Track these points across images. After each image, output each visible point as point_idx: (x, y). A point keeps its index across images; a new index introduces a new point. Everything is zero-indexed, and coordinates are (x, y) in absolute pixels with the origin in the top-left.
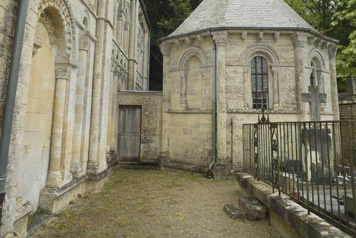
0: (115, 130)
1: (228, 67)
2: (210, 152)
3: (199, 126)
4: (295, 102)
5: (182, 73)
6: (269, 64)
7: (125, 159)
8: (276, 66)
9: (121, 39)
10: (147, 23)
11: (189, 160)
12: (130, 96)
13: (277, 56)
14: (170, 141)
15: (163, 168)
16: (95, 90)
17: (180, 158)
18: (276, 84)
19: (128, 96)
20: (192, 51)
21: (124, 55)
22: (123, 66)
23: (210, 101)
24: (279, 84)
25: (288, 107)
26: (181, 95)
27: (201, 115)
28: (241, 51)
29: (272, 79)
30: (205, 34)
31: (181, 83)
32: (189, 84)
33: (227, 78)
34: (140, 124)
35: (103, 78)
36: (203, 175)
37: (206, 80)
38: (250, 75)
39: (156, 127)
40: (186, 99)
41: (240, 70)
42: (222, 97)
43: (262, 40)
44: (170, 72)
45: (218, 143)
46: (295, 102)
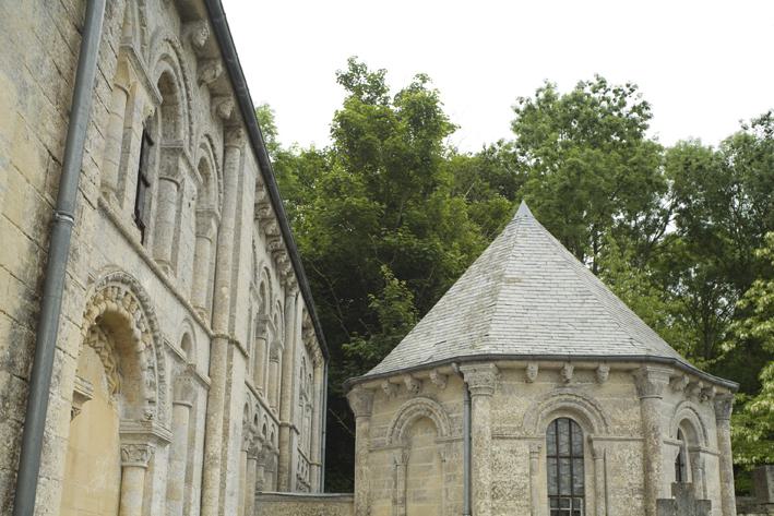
1: (496, 441)
5: (397, 454)
6: (586, 435)
8: (602, 439)
9: (264, 382)
12: (284, 504)
13: (603, 418)
16: (208, 492)
18: (600, 479)
21: (271, 415)
24: (608, 477)
26: (395, 502)
29: (591, 467)
30: (445, 370)
31: (395, 476)
32: (411, 478)
35: (224, 465)
37: (448, 469)
41: (523, 448)
43: (571, 383)
44: (371, 451)
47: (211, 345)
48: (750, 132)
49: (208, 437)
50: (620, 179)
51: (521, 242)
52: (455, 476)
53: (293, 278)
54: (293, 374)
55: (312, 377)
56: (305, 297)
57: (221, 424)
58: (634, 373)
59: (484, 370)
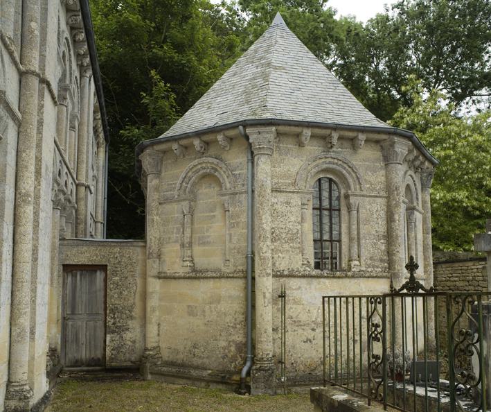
0: (57, 313)
1: (275, 194)
2: (241, 347)
3: (219, 301)
4: (385, 258)
5: (185, 206)
6: (343, 192)
7: (77, 363)
8: (357, 195)
9: (66, 143)
10: (105, 133)
11: (200, 362)
12: (85, 248)
13: (358, 178)
14: (161, 328)
15: (149, 377)
16: (21, 229)
17: (180, 358)
18: (354, 227)
19: (80, 248)
20: (204, 165)
21: (71, 174)
22: (69, 193)
23: (240, 256)
24: (361, 226)
25: (373, 267)
26: (183, 245)
27: (223, 280)
28: (298, 167)
29: (346, 218)
30: (231, 133)
32: (196, 226)
33: (275, 214)
34: (103, 300)
35: (37, 204)
36: (230, 387)
37: (232, 217)
38: (311, 211)
39: (134, 304)
40: (192, 252)
41: (296, 200)
42: (265, 248)
43: (334, 149)
44: (160, 204)
45: (257, 331)
46: (385, 258)
47: (20, 82)
48: (390, 14)
49: (20, 174)
50: (311, 33)
51: (280, 41)
52: (238, 223)
53: (88, 60)
54: (87, 143)
55: (97, 154)
56: (96, 85)
57: (33, 161)
58: (382, 144)
59: (267, 133)
